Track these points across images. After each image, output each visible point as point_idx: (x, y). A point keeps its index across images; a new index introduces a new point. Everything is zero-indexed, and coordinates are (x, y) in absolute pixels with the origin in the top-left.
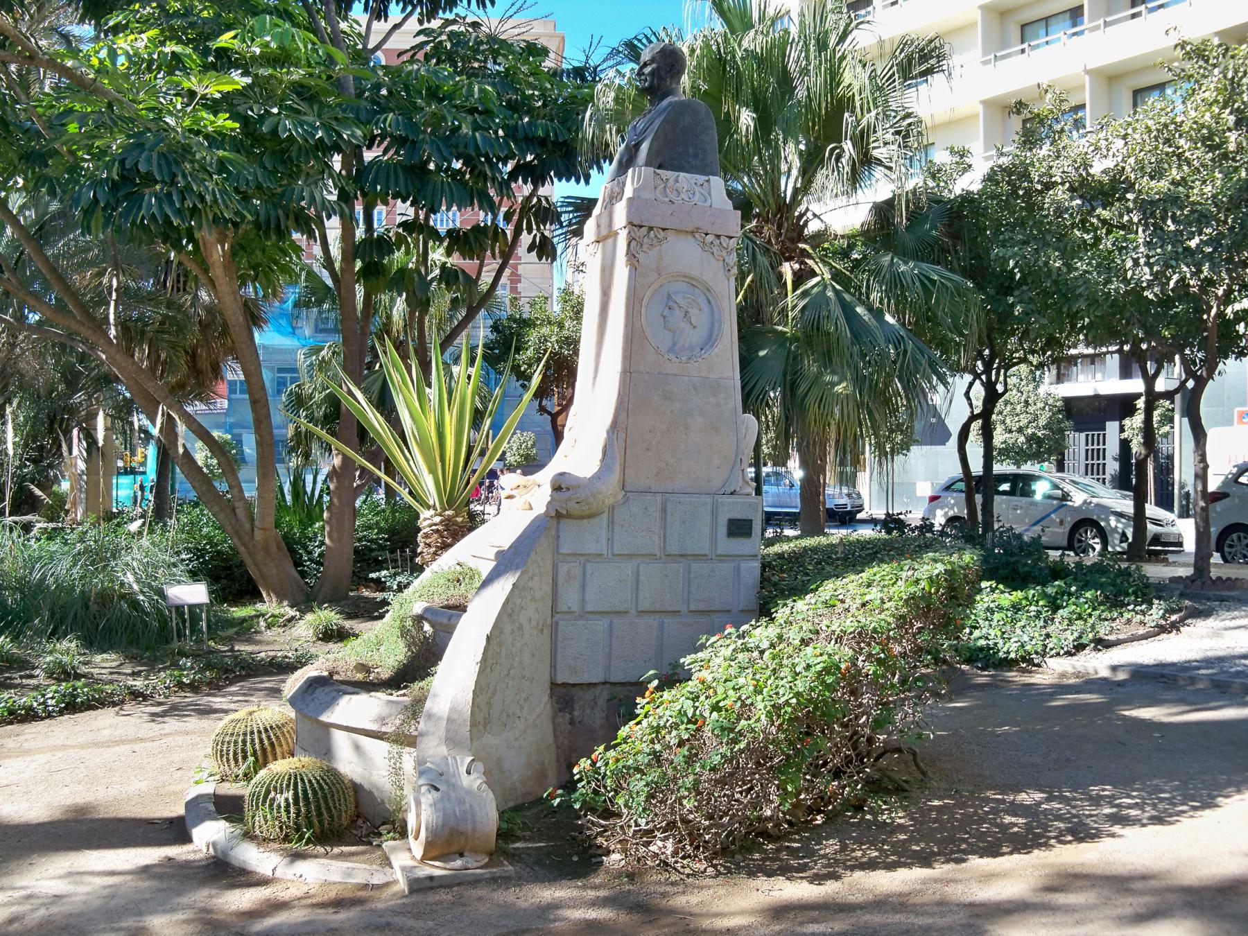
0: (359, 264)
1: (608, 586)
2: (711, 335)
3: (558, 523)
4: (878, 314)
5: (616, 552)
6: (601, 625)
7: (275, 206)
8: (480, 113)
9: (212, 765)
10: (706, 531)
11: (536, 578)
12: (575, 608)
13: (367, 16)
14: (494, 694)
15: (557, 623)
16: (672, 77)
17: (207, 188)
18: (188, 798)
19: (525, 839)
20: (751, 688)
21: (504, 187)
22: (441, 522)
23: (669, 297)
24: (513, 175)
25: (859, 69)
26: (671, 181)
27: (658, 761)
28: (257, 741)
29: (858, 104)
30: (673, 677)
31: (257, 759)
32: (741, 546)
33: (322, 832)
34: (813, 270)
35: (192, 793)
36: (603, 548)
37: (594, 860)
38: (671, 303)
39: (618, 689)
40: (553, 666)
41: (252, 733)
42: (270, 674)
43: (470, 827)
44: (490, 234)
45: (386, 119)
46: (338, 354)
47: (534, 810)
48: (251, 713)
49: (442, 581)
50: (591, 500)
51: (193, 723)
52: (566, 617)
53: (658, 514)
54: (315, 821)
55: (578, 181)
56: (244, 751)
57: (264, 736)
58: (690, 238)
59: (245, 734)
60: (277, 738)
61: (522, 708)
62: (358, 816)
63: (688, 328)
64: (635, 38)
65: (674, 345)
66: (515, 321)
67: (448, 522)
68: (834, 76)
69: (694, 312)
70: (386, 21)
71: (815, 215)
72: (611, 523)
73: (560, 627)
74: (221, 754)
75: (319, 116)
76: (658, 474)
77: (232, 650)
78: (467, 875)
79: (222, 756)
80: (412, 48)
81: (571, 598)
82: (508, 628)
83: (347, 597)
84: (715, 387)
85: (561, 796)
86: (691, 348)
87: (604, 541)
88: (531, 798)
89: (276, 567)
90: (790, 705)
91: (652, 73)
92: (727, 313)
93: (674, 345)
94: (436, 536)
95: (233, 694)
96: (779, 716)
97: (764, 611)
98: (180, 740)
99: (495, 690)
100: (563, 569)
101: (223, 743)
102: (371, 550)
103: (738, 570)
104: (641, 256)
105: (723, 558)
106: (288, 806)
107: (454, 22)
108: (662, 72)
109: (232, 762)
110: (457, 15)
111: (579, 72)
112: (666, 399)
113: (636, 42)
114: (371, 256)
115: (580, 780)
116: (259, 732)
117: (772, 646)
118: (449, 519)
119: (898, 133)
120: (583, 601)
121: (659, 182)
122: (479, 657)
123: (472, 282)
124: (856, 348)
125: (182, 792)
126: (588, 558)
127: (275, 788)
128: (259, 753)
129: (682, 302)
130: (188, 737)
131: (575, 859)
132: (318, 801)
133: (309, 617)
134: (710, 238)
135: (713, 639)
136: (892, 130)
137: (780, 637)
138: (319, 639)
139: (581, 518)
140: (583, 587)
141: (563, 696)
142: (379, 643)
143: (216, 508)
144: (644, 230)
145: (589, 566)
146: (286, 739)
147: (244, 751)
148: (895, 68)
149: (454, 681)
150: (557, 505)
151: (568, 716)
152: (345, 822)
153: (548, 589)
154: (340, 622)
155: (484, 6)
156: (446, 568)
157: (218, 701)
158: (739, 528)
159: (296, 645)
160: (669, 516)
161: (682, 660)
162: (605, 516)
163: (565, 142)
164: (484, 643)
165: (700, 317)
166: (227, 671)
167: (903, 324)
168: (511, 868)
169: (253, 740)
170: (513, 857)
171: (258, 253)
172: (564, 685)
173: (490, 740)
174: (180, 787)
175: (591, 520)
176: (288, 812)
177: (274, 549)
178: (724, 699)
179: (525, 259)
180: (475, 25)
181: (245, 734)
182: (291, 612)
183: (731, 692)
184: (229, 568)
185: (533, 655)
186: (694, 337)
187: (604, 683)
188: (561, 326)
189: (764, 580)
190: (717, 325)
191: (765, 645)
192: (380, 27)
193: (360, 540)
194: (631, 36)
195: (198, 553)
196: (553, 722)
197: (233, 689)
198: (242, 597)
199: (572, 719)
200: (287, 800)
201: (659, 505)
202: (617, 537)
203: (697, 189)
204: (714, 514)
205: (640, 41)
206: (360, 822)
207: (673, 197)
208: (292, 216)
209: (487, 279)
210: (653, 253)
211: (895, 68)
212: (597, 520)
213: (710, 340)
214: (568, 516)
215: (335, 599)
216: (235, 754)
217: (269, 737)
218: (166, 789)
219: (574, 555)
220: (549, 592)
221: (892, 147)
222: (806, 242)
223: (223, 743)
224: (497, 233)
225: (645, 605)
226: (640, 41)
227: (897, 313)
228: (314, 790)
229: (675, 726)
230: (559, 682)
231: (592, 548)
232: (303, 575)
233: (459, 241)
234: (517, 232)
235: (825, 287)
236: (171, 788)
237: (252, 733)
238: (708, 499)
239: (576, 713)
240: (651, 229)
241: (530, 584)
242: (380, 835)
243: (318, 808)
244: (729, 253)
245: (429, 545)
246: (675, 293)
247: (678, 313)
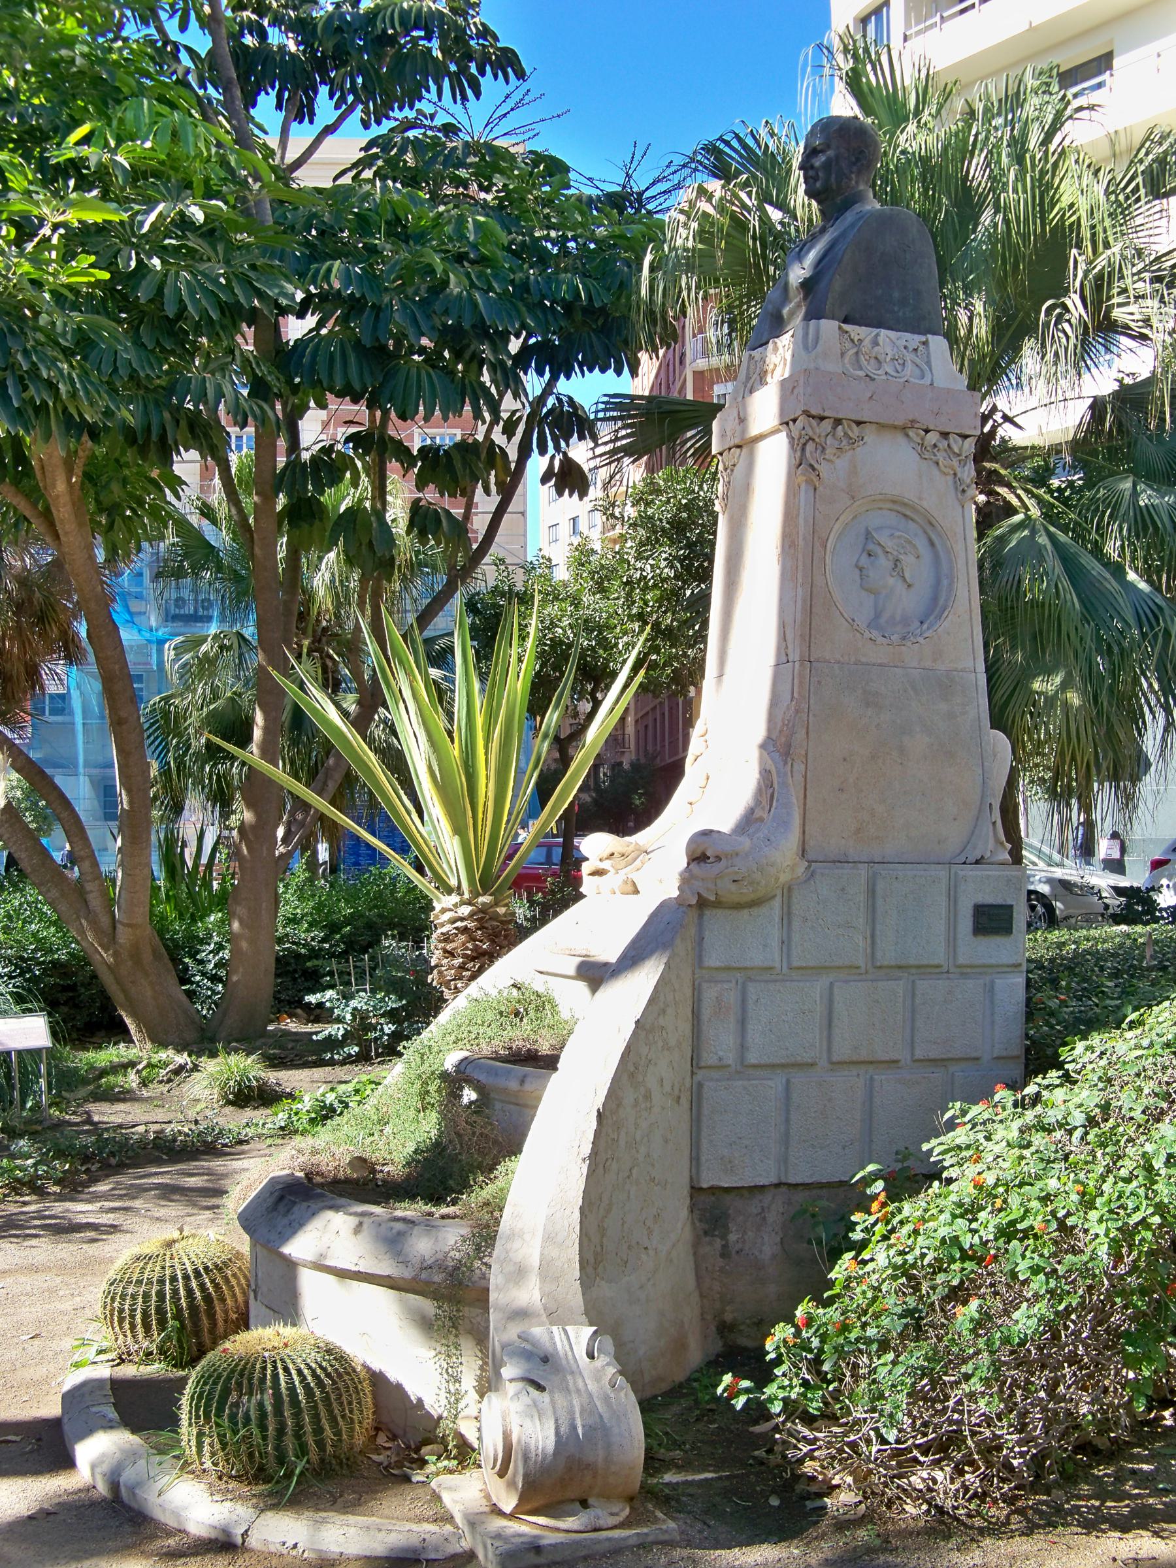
0: (281, 501)
1: (780, 1021)
2: (935, 599)
3: (701, 916)
4: (1118, 571)
5: (795, 964)
6: (774, 1085)
7: (157, 403)
8: (472, 262)
9: (103, 1336)
10: (941, 927)
11: (670, 1011)
12: (730, 1058)
13: (281, 116)
14: (608, 1211)
15: (700, 1085)
16: (859, 173)
17: (61, 371)
18: (67, 1387)
19: (680, 1468)
20: (1075, 1197)
21: (510, 380)
22: (472, 915)
23: (868, 535)
24: (523, 359)
25: (1087, 178)
26: (867, 342)
27: (918, 1328)
28: (182, 1292)
29: (1086, 233)
30: (912, 1177)
31: (182, 1323)
32: (995, 949)
33: (322, 1460)
34: (1008, 504)
35: (73, 1379)
36: (774, 957)
37: (810, 1504)
38: (871, 547)
39: (800, 1197)
40: (695, 1160)
41: (174, 1279)
42: (159, 1162)
43: (601, 1454)
44: (483, 456)
45: (329, 270)
46: (229, 648)
47: (676, 1409)
48: (170, 1244)
49: (490, 1016)
50: (757, 876)
51: (44, 1250)
52: (715, 1074)
53: (862, 897)
54: (310, 1440)
55: (619, 372)
56: (160, 1311)
57: (194, 1284)
58: (901, 439)
59: (161, 1281)
60: (217, 1286)
61: (650, 1232)
62: (377, 1429)
63: (900, 587)
64: (721, 139)
65: (877, 616)
66: (503, 594)
67: (483, 916)
68: (1045, 192)
69: (908, 561)
70: (311, 122)
71: (1006, 418)
72: (787, 915)
73: (705, 1089)
74: (118, 1316)
75: (227, 262)
76: (858, 831)
77: (89, 1121)
78: (599, 1541)
79: (121, 1320)
80: (354, 165)
81: (721, 1043)
82: (629, 1096)
83: (264, 1033)
84: (946, 685)
85: (747, 1391)
86: (905, 621)
87: (775, 944)
88: (664, 1387)
89: (152, 986)
90: (1148, 1227)
91: (827, 165)
92: (961, 562)
93: (877, 616)
94: (463, 938)
95: (97, 1197)
96: (1131, 1247)
97: (1040, 1057)
98: (25, 1282)
99: (610, 1205)
100: (710, 994)
101: (123, 1297)
102: (298, 956)
103: (990, 990)
104: (823, 468)
105: (966, 970)
106: (263, 1416)
107: (411, 125)
108: (843, 164)
109: (140, 1330)
110: (419, 112)
111: (617, 201)
112: (868, 705)
113: (722, 146)
114: (298, 495)
115: (778, 1361)
116: (186, 1277)
117: (1091, 1122)
118: (484, 910)
119: (1159, 279)
120: (743, 1047)
121: (848, 345)
122: (587, 1149)
123: (460, 528)
124: (1088, 629)
125: (47, 1380)
126: (747, 975)
127: (239, 1385)
128: (186, 1314)
129: (889, 544)
130: (41, 1277)
131: (774, 1502)
132: (315, 1407)
133: (210, 1066)
134: (932, 437)
135: (975, 1110)
136: (1147, 276)
137: (1105, 1107)
138: (229, 1103)
139: (738, 906)
140: (743, 1022)
141: (712, 1209)
142: (383, 1121)
143: (54, 893)
144: (827, 425)
145: (752, 988)
146: (231, 1288)
147: (160, 1311)
148: (1140, 179)
149: (543, 1187)
150: (698, 885)
151: (718, 1243)
152: (360, 1440)
153: (685, 1028)
154: (263, 1074)
155: (464, 98)
156: (494, 993)
157: (82, 1210)
158: (992, 920)
159: (192, 1114)
160: (879, 902)
161: (925, 1147)
162: (777, 903)
163: (603, 309)
164: (594, 1125)
165: (918, 568)
166: (87, 1159)
167: (1158, 589)
168: (672, 1525)
169: (175, 1292)
170: (667, 1500)
171: (115, 487)
172: (713, 1190)
173: (605, 1290)
174: (41, 1372)
175: (755, 911)
176: (263, 1427)
177: (147, 956)
178: (1023, 1218)
179: (535, 491)
180: (450, 130)
181: (161, 1281)
182: (182, 1059)
183: (1035, 1204)
184: (72, 988)
185: (666, 1141)
186: (908, 602)
187: (778, 1185)
188: (576, 602)
189: (1031, 1010)
190: (945, 582)
191: (1078, 1118)
192: (301, 136)
193: (280, 941)
194: (712, 137)
195: (21, 965)
196: (695, 1254)
197: (103, 1187)
198: (93, 1035)
199: (725, 1247)
200: (261, 1405)
201: (863, 880)
202: (796, 937)
203: (909, 357)
204: (953, 898)
205: (727, 143)
206: (382, 1439)
207: (871, 368)
208: (183, 423)
209: (479, 524)
210: (842, 463)
211: (1140, 179)
212: (763, 910)
213: (935, 606)
214: (718, 904)
215: (247, 1038)
216: (146, 1315)
217: (202, 1286)
218: (19, 1373)
219: (728, 969)
220: (688, 1032)
221: (1149, 302)
222: (994, 459)
223: (123, 1297)
224: (491, 455)
225: (842, 1051)
226: (727, 143)
227: (1148, 574)
228: (307, 1387)
229: (938, 1267)
230: (705, 1186)
231: (756, 957)
232: (191, 994)
233: (437, 466)
234: (524, 452)
235: (1034, 532)
236: (28, 1374)
237: (174, 1279)
238: (942, 873)
239: (732, 1237)
240: (838, 422)
241: (661, 1021)
242: (423, 1463)
243: (316, 1417)
244: (962, 463)
245: (451, 954)
246: (878, 529)
247: (884, 563)
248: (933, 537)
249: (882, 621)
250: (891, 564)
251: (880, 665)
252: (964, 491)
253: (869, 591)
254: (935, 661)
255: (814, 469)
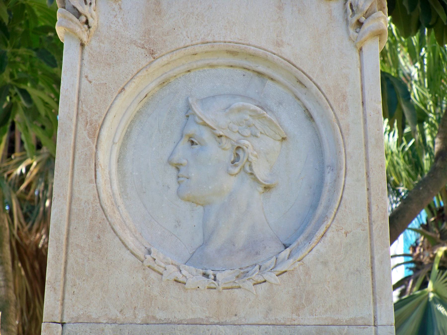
38: (193, 129)
86: (253, 248)
186: (265, 214)
190: (328, 178)
247: (217, 153)
248: (309, 105)
249: (211, 249)
250: (229, 156)
251: (193, 323)
252: (360, 24)
253: (192, 201)
254: (297, 309)
255: (78, 14)
